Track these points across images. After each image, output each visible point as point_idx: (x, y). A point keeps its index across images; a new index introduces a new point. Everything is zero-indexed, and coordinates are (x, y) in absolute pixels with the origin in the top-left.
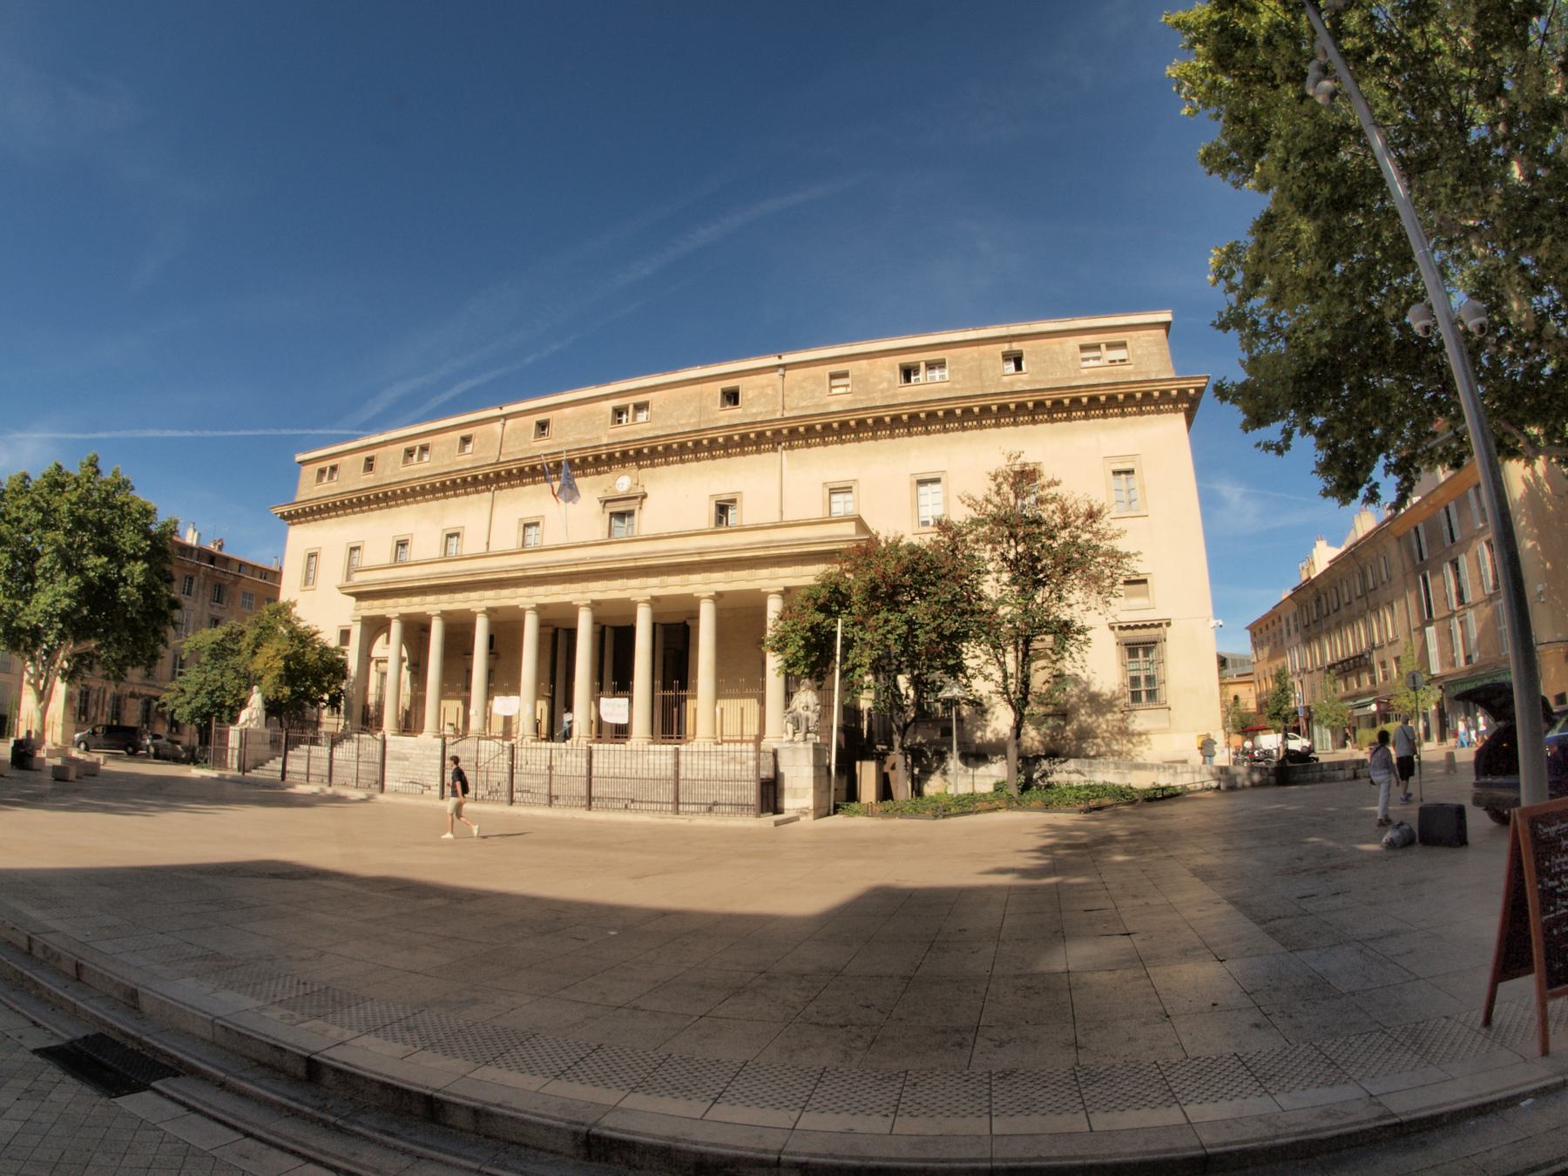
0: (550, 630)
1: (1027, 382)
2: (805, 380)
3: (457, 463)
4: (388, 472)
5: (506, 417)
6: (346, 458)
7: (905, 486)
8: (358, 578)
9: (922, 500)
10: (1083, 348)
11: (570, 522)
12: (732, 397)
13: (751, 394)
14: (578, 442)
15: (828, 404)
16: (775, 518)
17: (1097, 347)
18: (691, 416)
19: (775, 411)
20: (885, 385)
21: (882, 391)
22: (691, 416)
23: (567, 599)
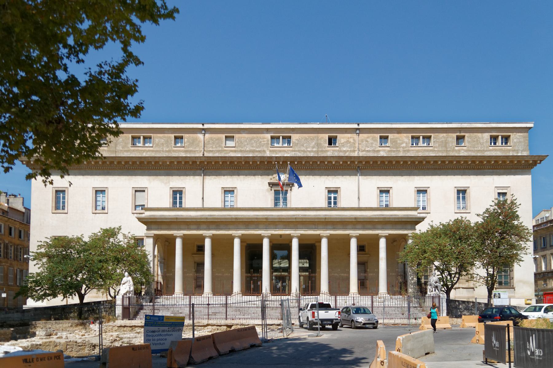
0: (245, 244)
1: (466, 151)
2: (368, 137)
3: (174, 151)
4: (119, 148)
5: (205, 131)
8: (147, 214)
9: (98, 199)
11: (253, 193)
12: (331, 141)
14: (253, 151)
15: (379, 151)
16: (200, 206)
18: (313, 147)
19: (354, 151)
20: (404, 145)
21: (403, 147)
22: (313, 147)
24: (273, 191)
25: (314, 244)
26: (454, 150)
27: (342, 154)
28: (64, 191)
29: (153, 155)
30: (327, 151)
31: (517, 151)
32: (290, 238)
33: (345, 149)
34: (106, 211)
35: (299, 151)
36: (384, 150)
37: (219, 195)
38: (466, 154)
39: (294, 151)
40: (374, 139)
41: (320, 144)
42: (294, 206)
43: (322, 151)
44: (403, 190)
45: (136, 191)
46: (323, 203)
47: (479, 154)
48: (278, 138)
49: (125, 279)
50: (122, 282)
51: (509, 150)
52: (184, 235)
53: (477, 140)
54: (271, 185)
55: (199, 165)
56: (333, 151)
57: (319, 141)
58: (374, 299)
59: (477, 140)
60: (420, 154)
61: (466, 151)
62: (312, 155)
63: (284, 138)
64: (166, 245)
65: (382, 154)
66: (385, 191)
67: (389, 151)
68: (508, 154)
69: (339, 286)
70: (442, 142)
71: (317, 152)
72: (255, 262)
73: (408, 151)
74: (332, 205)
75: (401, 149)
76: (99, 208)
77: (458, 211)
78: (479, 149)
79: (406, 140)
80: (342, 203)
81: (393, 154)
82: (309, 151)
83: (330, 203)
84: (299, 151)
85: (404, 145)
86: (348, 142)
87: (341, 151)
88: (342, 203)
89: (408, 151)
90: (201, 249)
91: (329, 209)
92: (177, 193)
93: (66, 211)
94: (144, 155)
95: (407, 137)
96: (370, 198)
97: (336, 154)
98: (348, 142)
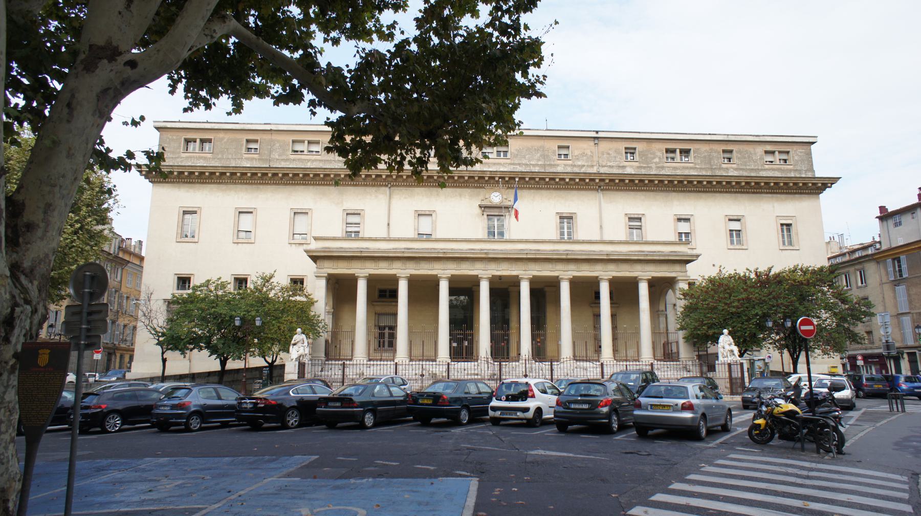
6: (221, 135)
7: (175, 217)
10: (767, 152)
13: (576, 153)
15: (624, 167)
16: (384, 235)
17: (773, 153)
19: (592, 166)
20: (657, 160)
21: (656, 163)
23: (514, 273)
24: (485, 216)
25: (507, 289)
26: (721, 168)
27: (576, 170)
28: (571, 218)
29: (321, 165)
30: (558, 165)
31: (800, 171)
32: (394, 280)
33: (580, 163)
34: (196, 239)
35: (519, 164)
36: (631, 167)
37: (410, 219)
38: (736, 173)
39: (513, 164)
40: (617, 151)
41: (548, 156)
42: (514, 237)
43: (550, 165)
44: (660, 218)
45: (295, 213)
46: (554, 235)
47: (753, 174)
48: (673, 151)
49: (296, 338)
50: (293, 342)
51: (791, 170)
52: (329, 275)
53: (749, 157)
54: (484, 208)
55: (385, 180)
56: (565, 165)
57: (546, 153)
58: (555, 367)
59: (749, 157)
60: (679, 172)
61: (736, 169)
62: (537, 169)
63: (682, 151)
64: (341, 290)
65: (629, 171)
66: (567, 218)
67: (638, 167)
68: (789, 175)
69: (502, 349)
70: (705, 157)
71: (544, 166)
72: (460, 315)
73: (663, 168)
74: (566, 237)
75: (653, 166)
76: (242, 237)
77: (732, 247)
78: (752, 167)
79: (659, 154)
80: (580, 235)
81: (643, 172)
82: (534, 165)
83: (562, 234)
84: (519, 164)
85: (657, 160)
86: (583, 154)
87: (575, 166)
88: (580, 235)
89: (663, 168)
90: (393, 294)
91: (680, 242)
92: (635, 220)
93: (196, 239)
94: (309, 165)
95: (660, 150)
96: (617, 229)
97: (569, 170)
98: (583, 154)
